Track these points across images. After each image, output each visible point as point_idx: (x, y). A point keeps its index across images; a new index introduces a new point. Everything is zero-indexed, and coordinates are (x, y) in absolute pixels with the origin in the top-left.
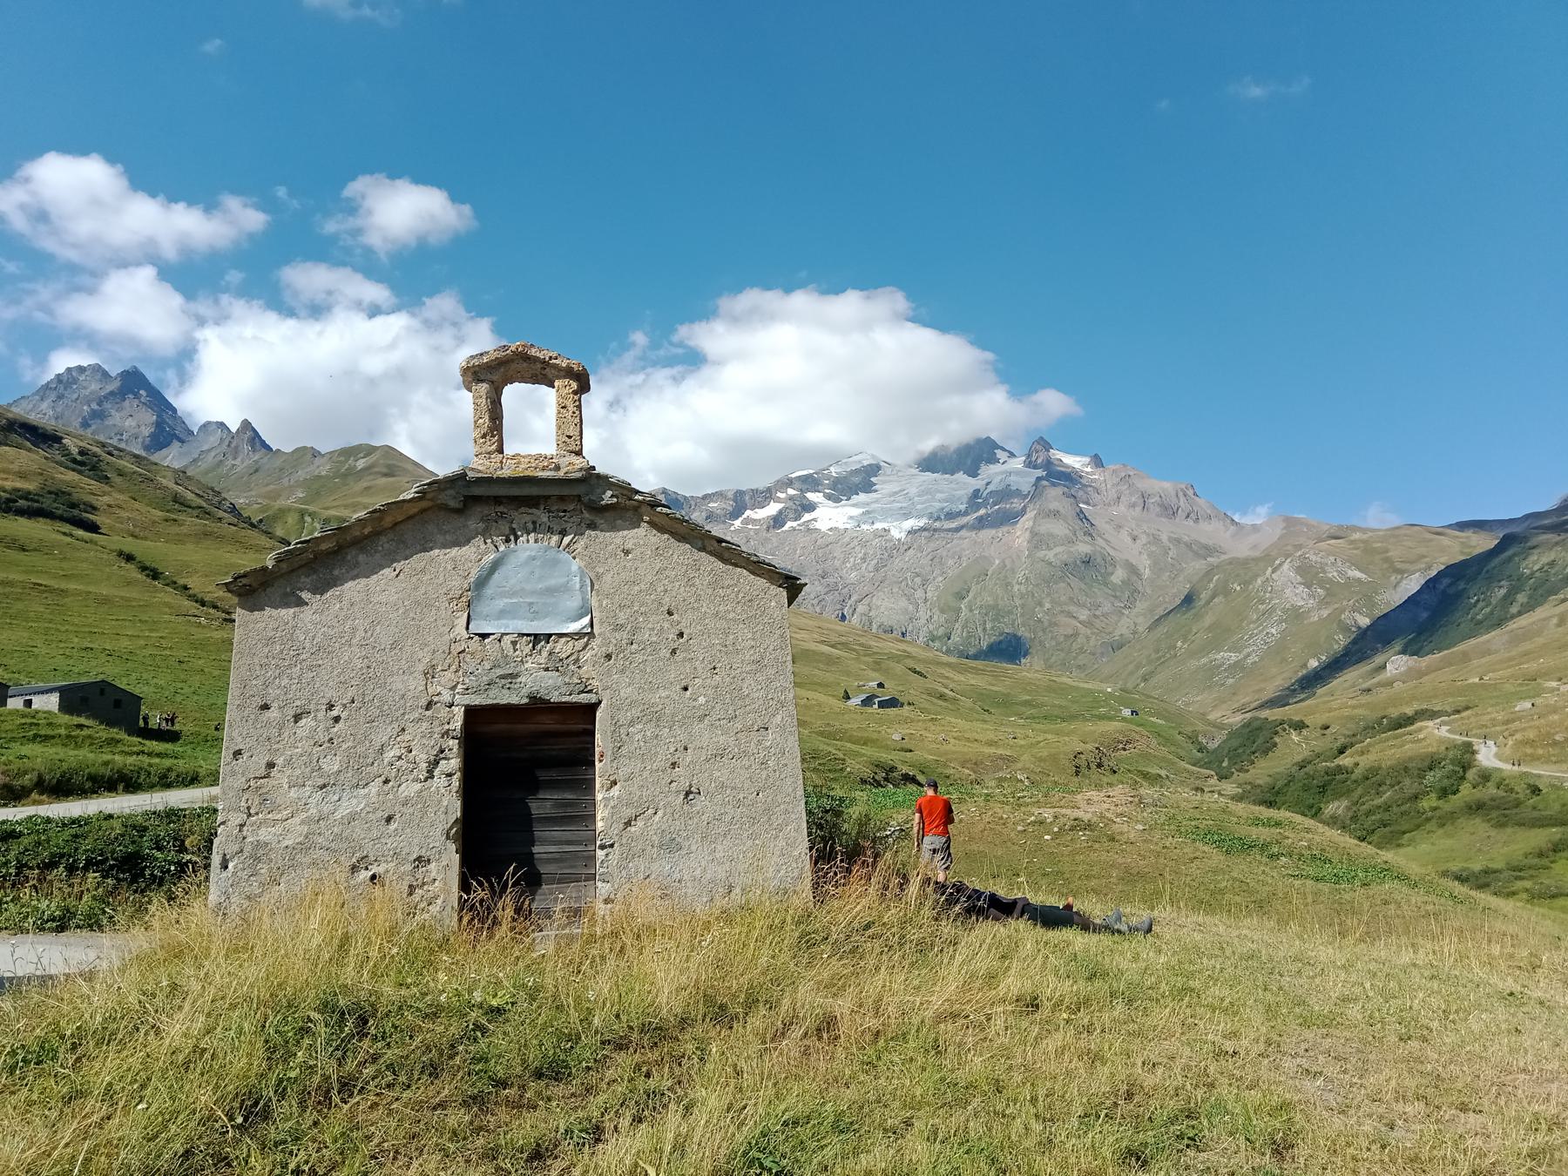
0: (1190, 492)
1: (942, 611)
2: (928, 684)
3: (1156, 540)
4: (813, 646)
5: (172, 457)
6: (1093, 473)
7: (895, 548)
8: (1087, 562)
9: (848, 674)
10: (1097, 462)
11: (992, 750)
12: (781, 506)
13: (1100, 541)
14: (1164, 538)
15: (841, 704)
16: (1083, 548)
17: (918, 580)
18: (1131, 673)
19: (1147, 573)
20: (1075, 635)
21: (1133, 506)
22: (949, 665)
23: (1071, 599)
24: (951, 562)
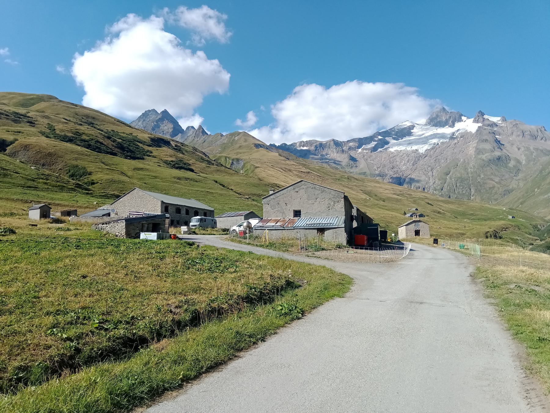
0: (543, 129)
1: (439, 180)
2: (434, 208)
3: (528, 149)
4: (391, 196)
5: (178, 138)
6: (501, 124)
7: (420, 156)
8: (499, 158)
9: (404, 205)
10: (504, 120)
11: (456, 231)
12: (376, 143)
13: (504, 150)
14: (532, 148)
15: (403, 216)
16: (497, 153)
17: (430, 168)
18: (516, 202)
19: (524, 162)
20: (494, 187)
21: (519, 136)
22: (442, 201)
23: (492, 173)
24: (443, 161)
